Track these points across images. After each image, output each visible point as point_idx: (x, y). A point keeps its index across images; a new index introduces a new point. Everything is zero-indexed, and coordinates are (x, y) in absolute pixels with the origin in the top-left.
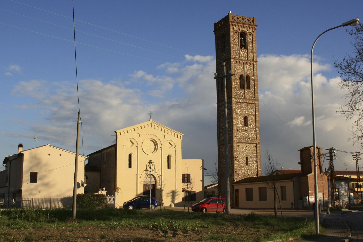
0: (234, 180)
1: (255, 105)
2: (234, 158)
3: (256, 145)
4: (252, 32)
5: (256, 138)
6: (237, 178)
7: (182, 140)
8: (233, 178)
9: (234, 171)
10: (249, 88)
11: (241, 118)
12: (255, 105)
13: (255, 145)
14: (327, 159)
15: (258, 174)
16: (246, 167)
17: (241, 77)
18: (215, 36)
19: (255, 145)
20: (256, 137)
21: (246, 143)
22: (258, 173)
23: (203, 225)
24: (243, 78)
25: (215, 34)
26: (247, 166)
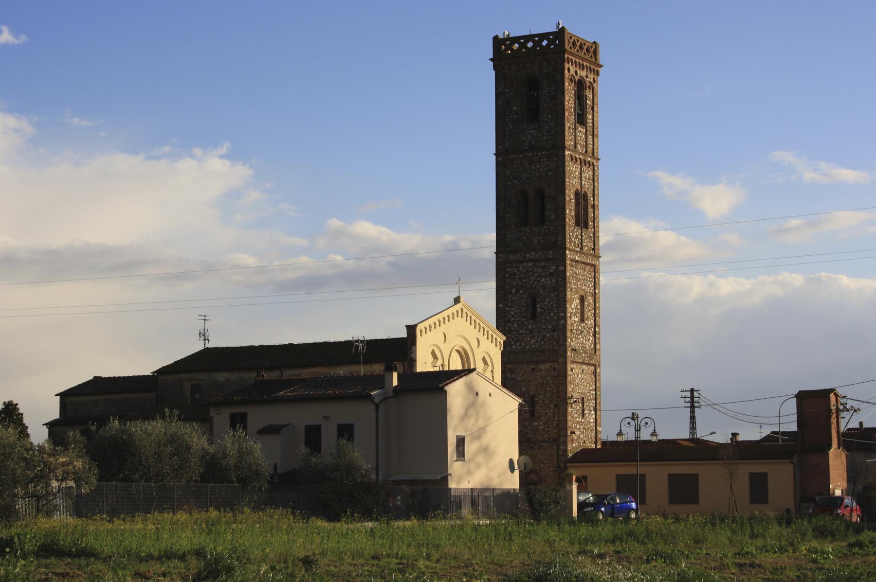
0: (568, 453)
1: (594, 270)
2: (694, 397)
3: (595, 369)
4: (585, 78)
5: (595, 352)
6: (573, 447)
7: (501, 352)
8: (562, 447)
9: (569, 432)
10: (586, 226)
11: (576, 301)
12: (594, 270)
13: (593, 368)
14: (44, 423)
15: (598, 440)
16: (581, 422)
17: (577, 193)
18: (494, 72)
19: (593, 368)
20: (595, 349)
21: (583, 363)
22: (598, 437)
23: (781, 526)
24: (579, 200)
25: (495, 68)
26: (583, 420)
